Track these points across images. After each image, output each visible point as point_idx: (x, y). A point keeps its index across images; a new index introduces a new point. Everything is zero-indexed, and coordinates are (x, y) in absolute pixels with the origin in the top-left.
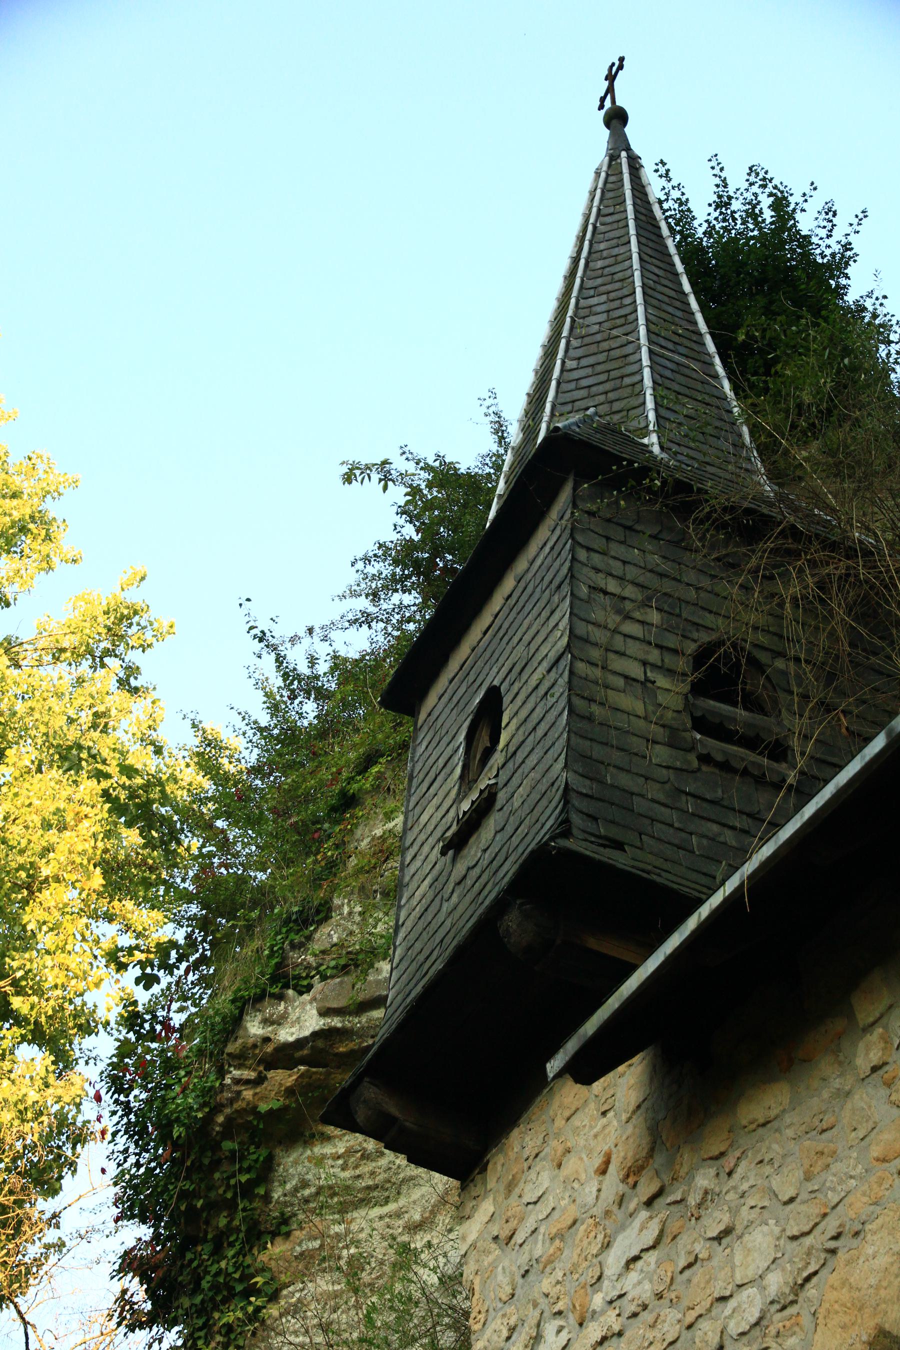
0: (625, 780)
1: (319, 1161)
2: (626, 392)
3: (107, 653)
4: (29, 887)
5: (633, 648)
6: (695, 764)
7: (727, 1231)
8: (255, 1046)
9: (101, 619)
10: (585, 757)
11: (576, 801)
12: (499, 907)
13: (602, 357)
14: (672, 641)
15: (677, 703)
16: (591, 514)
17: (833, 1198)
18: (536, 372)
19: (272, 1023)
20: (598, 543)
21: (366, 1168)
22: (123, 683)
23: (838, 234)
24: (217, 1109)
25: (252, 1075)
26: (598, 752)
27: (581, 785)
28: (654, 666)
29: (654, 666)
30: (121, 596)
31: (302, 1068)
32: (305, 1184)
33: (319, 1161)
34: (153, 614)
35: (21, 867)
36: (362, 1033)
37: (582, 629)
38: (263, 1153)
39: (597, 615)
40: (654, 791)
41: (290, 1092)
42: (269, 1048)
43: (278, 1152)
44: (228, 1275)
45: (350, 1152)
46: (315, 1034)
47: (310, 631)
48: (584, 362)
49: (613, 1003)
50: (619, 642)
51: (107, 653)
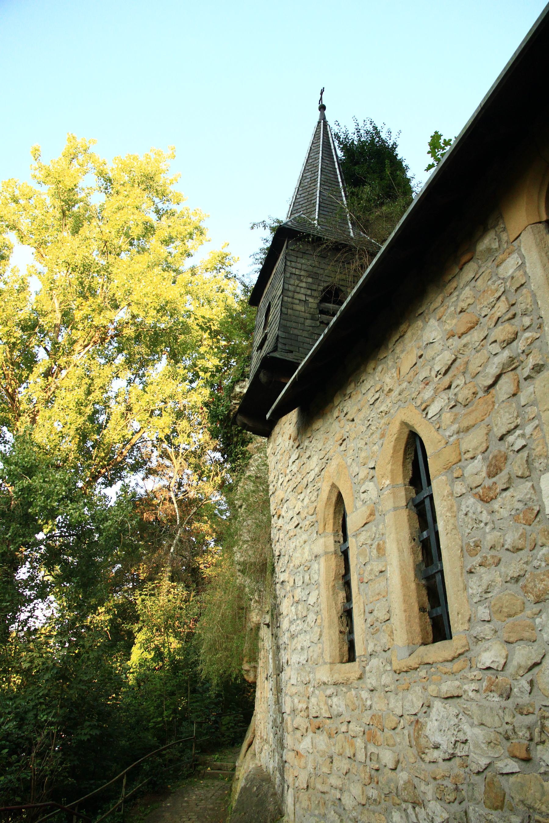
0: (296, 332)
2: (312, 206)
3: (220, 268)
4: (201, 341)
5: (303, 291)
6: (319, 324)
7: (310, 457)
9: (217, 258)
10: (285, 326)
11: (280, 340)
13: (307, 194)
14: (314, 287)
15: (315, 306)
16: (293, 250)
17: (328, 450)
20: (294, 259)
22: (226, 276)
23: (393, 139)
24: (231, 411)
26: (289, 324)
27: (281, 334)
28: (309, 296)
29: (309, 296)
30: (222, 251)
34: (232, 255)
35: (198, 336)
37: (286, 286)
39: (292, 282)
40: (305, 334)
47: (243, 276)
48: (302, 196)
49: (277, 401)
50: (298, 289)
51: (220, 268)
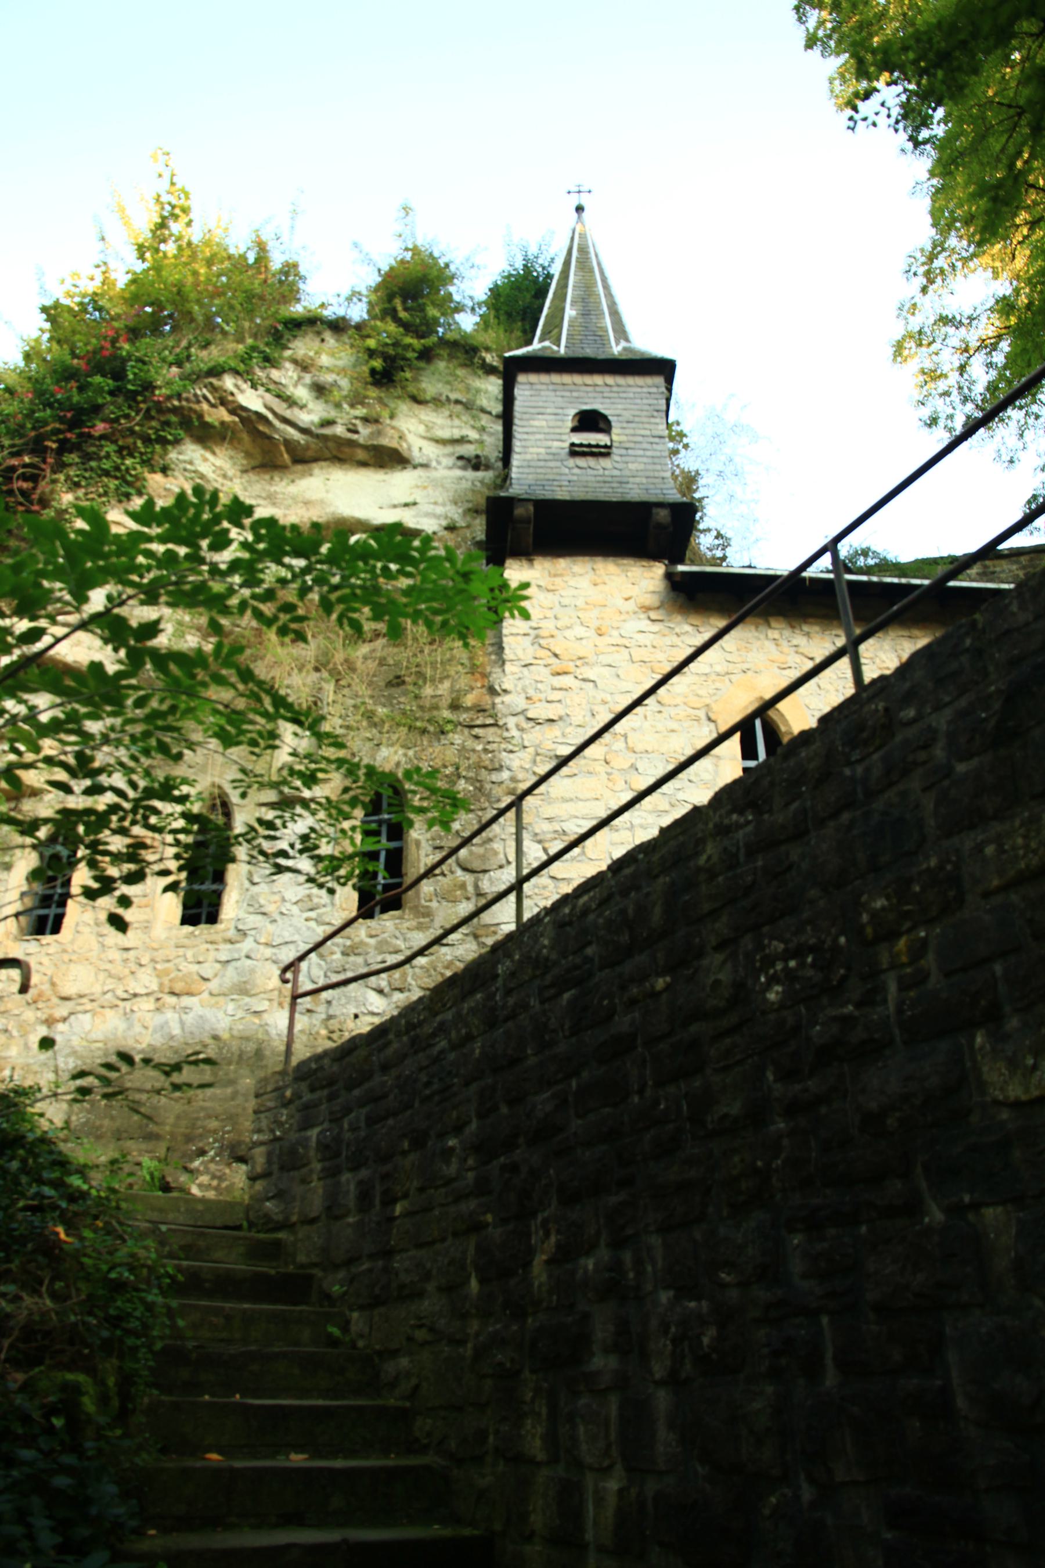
1: (206, 460)
12: (660, 505)
18: (531, 561)
25: (213, 401)
31: (237, 419)
32: (191, 463)
36: (276, 430)
38: (181, 432)
41: (223, 423)
42: (230, 398)
43: (188, 440)
45: (221, 468)
46: (257, 413)
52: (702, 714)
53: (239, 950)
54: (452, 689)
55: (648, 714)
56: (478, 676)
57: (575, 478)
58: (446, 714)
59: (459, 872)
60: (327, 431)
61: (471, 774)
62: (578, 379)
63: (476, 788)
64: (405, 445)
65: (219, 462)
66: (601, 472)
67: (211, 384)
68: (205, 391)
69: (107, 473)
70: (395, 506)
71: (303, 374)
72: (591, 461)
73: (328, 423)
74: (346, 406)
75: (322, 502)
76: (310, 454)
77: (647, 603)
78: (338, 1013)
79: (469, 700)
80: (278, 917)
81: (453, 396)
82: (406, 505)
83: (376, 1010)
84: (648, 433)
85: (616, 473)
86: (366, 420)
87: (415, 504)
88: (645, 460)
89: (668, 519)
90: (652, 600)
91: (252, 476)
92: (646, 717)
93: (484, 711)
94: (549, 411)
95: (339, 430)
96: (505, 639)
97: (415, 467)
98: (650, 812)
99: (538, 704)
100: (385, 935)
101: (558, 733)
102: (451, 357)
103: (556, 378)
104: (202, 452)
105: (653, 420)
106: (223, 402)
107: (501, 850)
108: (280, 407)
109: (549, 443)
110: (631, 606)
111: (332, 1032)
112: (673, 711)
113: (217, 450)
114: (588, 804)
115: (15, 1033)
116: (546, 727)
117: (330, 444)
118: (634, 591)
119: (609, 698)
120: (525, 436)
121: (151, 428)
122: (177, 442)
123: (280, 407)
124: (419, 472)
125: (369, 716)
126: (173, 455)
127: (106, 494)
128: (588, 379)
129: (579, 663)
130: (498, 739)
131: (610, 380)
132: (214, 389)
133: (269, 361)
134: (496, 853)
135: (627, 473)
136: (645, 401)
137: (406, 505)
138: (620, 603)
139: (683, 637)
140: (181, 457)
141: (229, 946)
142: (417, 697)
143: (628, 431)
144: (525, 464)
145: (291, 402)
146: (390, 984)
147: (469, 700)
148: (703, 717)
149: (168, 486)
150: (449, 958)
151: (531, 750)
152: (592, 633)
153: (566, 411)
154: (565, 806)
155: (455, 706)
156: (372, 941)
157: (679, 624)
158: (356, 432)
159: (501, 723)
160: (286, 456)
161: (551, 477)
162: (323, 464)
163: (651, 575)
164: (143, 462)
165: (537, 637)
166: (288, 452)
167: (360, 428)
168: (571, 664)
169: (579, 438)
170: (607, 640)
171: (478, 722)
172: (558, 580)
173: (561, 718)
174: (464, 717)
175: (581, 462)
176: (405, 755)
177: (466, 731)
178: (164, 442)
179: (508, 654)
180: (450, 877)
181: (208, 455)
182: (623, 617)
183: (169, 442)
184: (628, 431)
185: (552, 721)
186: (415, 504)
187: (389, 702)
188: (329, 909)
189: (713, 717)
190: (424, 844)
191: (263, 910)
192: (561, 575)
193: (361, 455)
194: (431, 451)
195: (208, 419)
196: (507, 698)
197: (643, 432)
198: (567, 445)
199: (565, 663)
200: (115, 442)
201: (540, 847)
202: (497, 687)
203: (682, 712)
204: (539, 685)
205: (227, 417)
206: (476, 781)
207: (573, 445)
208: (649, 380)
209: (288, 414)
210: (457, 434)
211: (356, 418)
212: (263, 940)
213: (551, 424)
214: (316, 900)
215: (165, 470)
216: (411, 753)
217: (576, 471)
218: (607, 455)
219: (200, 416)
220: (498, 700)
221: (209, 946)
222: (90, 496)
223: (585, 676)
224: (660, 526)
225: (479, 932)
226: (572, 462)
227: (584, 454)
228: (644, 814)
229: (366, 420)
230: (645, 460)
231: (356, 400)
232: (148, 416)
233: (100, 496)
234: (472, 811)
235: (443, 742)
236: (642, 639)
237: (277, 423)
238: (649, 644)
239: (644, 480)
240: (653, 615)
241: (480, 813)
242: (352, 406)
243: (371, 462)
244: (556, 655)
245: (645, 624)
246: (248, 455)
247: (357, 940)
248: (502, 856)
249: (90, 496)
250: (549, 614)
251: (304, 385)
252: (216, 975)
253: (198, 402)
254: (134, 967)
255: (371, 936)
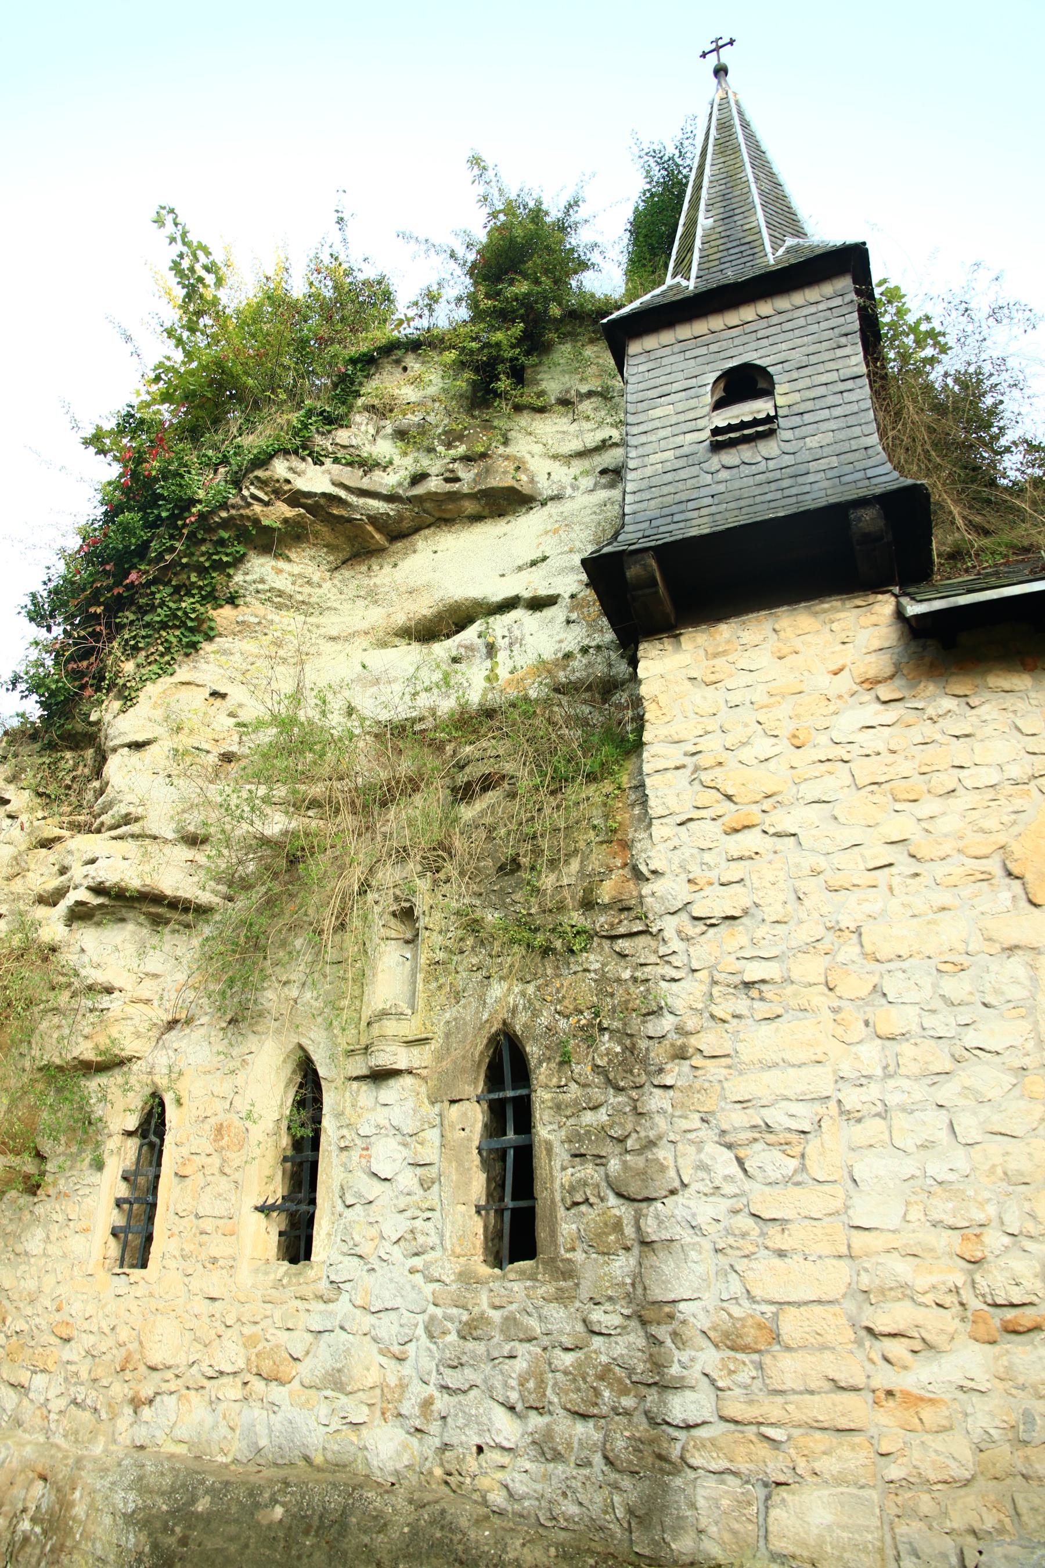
1: (279, 571)
8: (278, 481)
19: (295, 472)
21: (307, 589)
25: (266, 498)
31: (302, 511)
32: (262, 581)
33: (279, 571)
38: (241, 549)
41: (286, 521)
42: (287, 487)
43: (252, 554)
44: (186, 613)
45: (301, 576)
46: (324, 495)
52: (993, 865)
53: (331, 1314)
54: (582, 873)
55: (896, 881)
56: (616, 847)
57: (721, 488)
58: (576, 918)
59: (612, 1200)
60: (419, 490)
61: (616, 1024)
62: (716, 322)
63: (625, 1048)
64: (524, 478)
65: (296, 569)
66: (762, 467)
67: (257, 477)
68: (253, 489)
69: (164, 626)
70: (520, 569)
71: (382, 423)
72: (745, 452)
73: (418, 478)
74: (440, 449)
75: (428, 586)
76: (406, 524)
77: (871, 674)
78: (454, 1441)
79: (606, 893)
80: (376, 1264)
81: (584, 389)
82: (534, 563)
83: (506, 1444)
84: (833, 376)
85: (788, 460)
86: (467, 459)
87: (544, 559)
88: (833, 425)
89: (881, 523)
90: (879, 664)
91: (346, 573)
92: (891, 889)
93: (629, 909)
94: (676, 387)
95: (434, 484)
96: (648, 781)
97: (544, 504)
98: (917, 1078)
99: (708, 891)
100: (513, 1307)
101: (744, 940)
102: (573, 336)
103: (684, 332)
104: (273, 563)
105: (839, 353)
106: (277, 493)
107: (670, 1163)
108: (353, 477)
109: (679, 441)
110: (845, 683)
111: (450, 1474)
112: (940, 870)
113: (293, 555)
114: (804, 1070)
115: (104, 1416)
116: (724, 928)
117: (428, 505)
118: (848, 655)
119: (822, 863)
120: (643, 439)
121: (203, 554)
122: (239, 560)
123: (353, 477)
124: (551, 508)
125: (474, 926)
126: (238, 578)
127: (168, 650)
128: (732, 318)
129: (767, 805)
130: (653, 959)
131: (765, 308)
132: (263, 483)
133: (332, 421)
134: (663, 1169)
135: (806, 456)
136: (824, 325)
137: (534, 563)
138: (824, 681)
139: (942, 723)
140: (248, 578)
141: (322, 1306)
142: (536, 891)
143: (800, 384)
144: (644, 484)
145: (368, 465)
146: (522, 1398)
147: (606, 893)
148: (998, 872)
149: (240, 619)
150: (604, 1359)
151: (702, 975)
152: (784, 745)
153: (701, 381)
154: (767, 1076)
155: (588, 904)
156: (496, 1316)
157: (933, 698)
158: (457, 480)
159: (654, 930)
160: (377, 536)
161: (683, 497)
162: (427, 532)
163: (874, 619)
164: (204, 599)
165: (696, 769)
166: (378, 530)
167: (461, 474)
168: (756, 809)
169: (723, 418)
170: (810, 754)
171: (622, 930)
172: (719, 662)
173: (746, 912)
174: (602, 921)
175: (729, 457)
176: (523, 994)
177: (606, 944)
178: (220, 567)
179: (656, 808)
180: (600, 1207)
181: (281, 564)
182: (832, 708)
183: (228, 565)
184: (800, 384)
185: (733, 918)
186: (544, 559)
187: (501, 900)
188: (438, 1254)
189: (1016, 871)
190: (558, 1149)
191: (358, 1250)
192: (724, 653)
193: (470, 507)
194: (563, 474)
195: (265, 522)
196: (657, 886)
197: (824, 378)
198: (707, 433)
199: (746, 809)
200: (168, 583)
201: (729, 1155)
202: (643, 868)
203: (957, 868)
204: (707, 857)
205: (289, 512)
206: (624, 1035)
207: (716, 431)
208: (828, 289)
209: (365, 484)
210: (592, 439)
211: (454, 460)
212: (358, 1303)
213: (680, 407)
214: (421, 1239)
215: (232, 600)
216: (531, 989)
217: (724, 474)
218: (771, 433)
219: (256, 522)
220: (646, 889)
221: (299, 1302)
222: (152, 658)
223: (779, 829)
224: (868, 538)
225: (647, 1314)
226: (716, 461)
227: (732, 443)
228: (905, 1083)
229: (467, 459)
230: (833, 425)
231: (451, 438)
232: (193, 540)
233: (162, 655)
234: (622, 1089)
235: (574, 968)
236: (870, 741)
237: (352, 499)
238: (881, 747)
239: (834, 461)
240: (885, 692)
241: (634, 1094)
242: (449, 446)
243: (486, 513)
244: (729, 797)
245: (874, 713)
246: (331, 548)
247: (476, 1310)
248: (672, 1173)
249: (152, 658)
250: (712, 725)
251: (385, 437)
252: (307, 1353)
253: (249, 505)
254: (221, 1329)
255: (496, 1308)
